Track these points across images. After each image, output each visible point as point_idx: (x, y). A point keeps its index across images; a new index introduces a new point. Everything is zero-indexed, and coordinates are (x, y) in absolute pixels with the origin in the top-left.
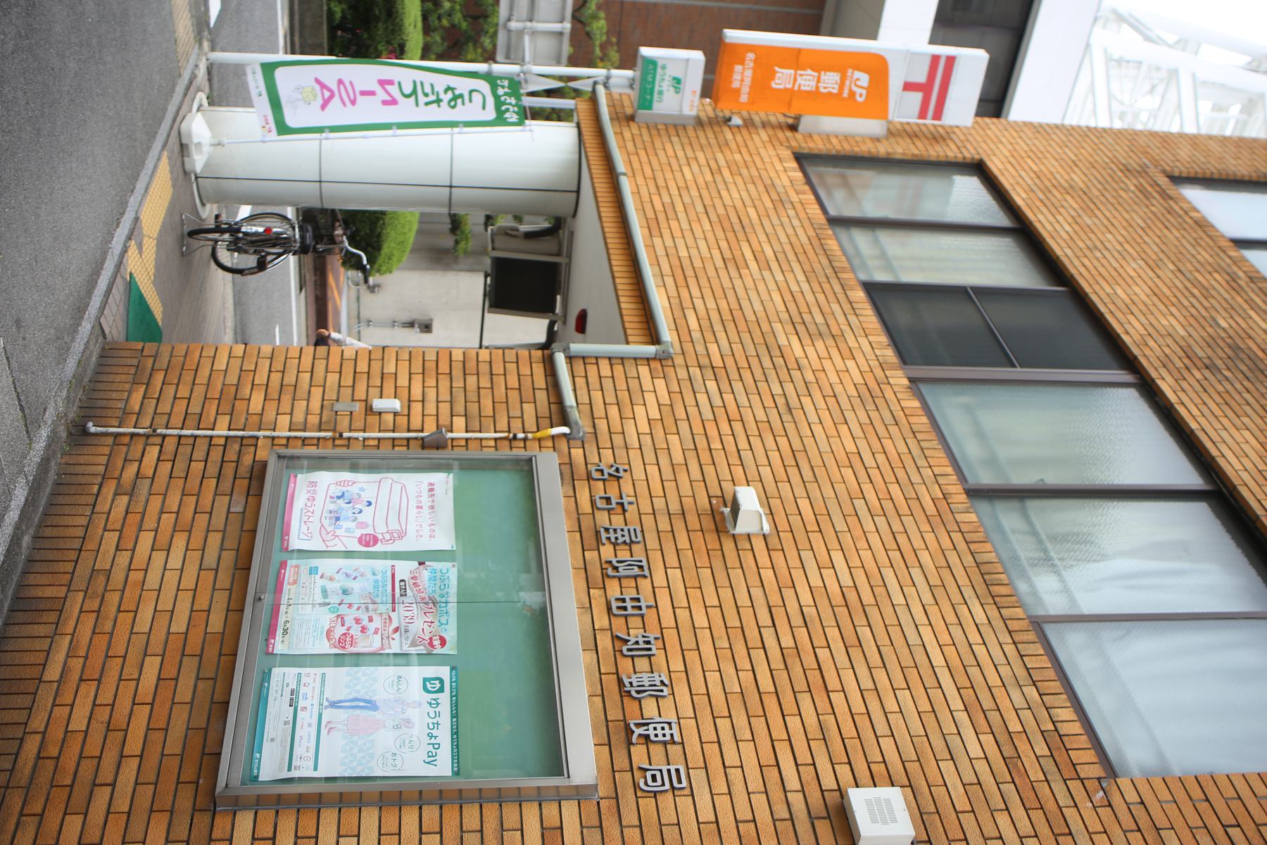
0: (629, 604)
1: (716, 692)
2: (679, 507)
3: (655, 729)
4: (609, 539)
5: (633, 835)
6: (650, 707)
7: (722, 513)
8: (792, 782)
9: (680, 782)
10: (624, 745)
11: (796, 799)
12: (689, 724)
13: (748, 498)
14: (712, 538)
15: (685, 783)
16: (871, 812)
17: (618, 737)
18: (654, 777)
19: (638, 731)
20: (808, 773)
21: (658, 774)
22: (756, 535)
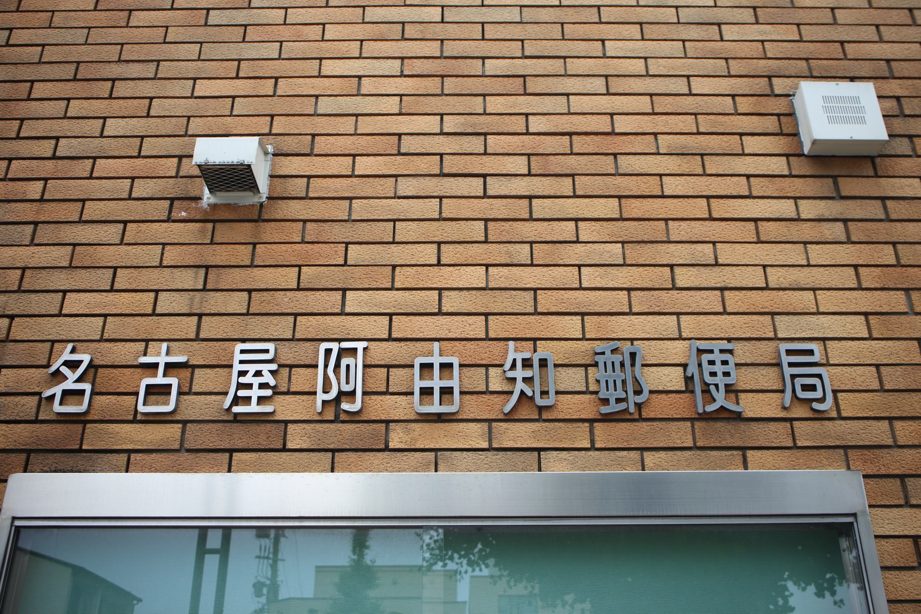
0: (436, 383)
1: (623, 277)
2: (191, 272)
3: (713, 374)
4: (261, 400)
5: (905, 432)
6: (654, 379)
7: (214, 207)
8: (786, 208)
9: (267, 351)
10: (743, 426)
11: (808, 209)
12: (689, 325)
13: (212, 151)
14: (270, 232)
15: (270, 346)
16: (847, 120)
17: (727, 433)
18: (805, 388)
19: (721, 399)
20: (758, 186)
21: (799, 382)
22: (273, 165)
